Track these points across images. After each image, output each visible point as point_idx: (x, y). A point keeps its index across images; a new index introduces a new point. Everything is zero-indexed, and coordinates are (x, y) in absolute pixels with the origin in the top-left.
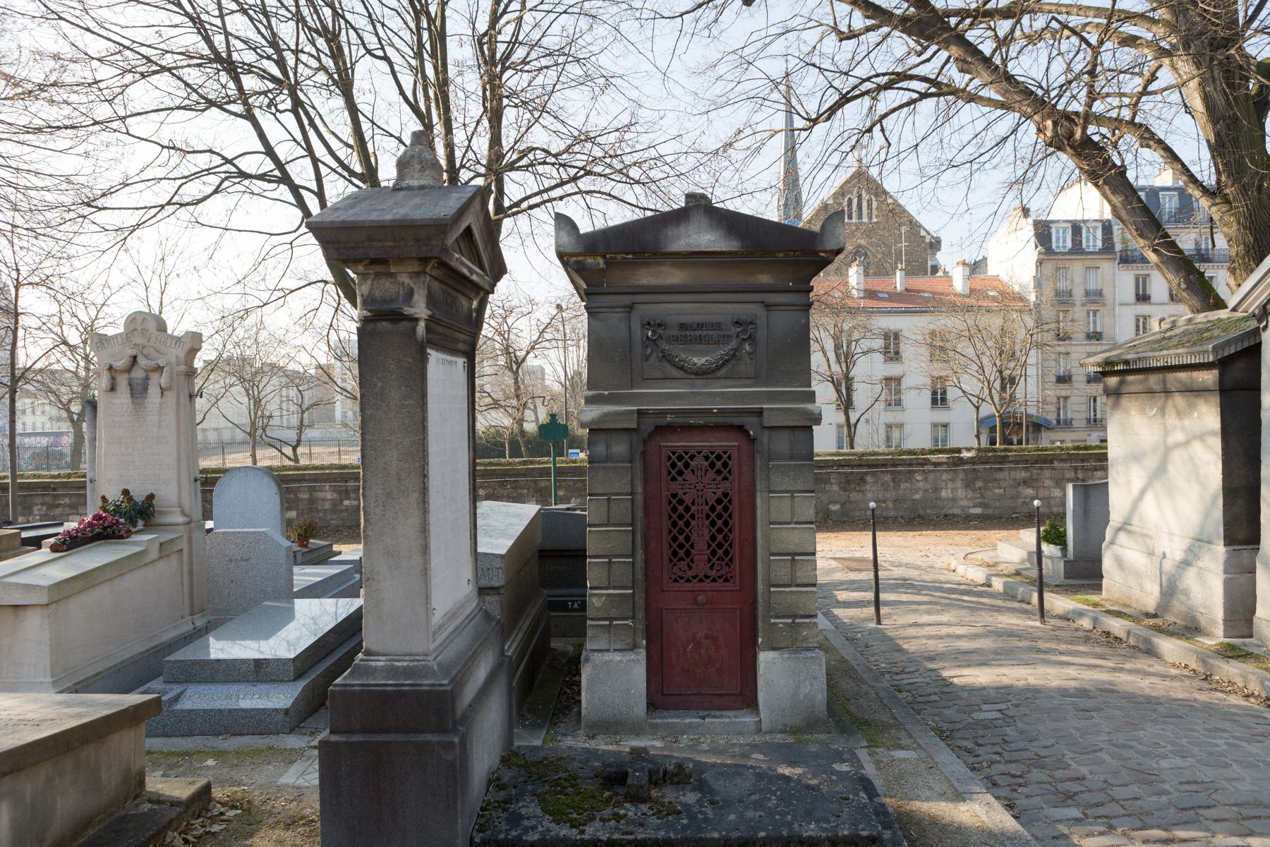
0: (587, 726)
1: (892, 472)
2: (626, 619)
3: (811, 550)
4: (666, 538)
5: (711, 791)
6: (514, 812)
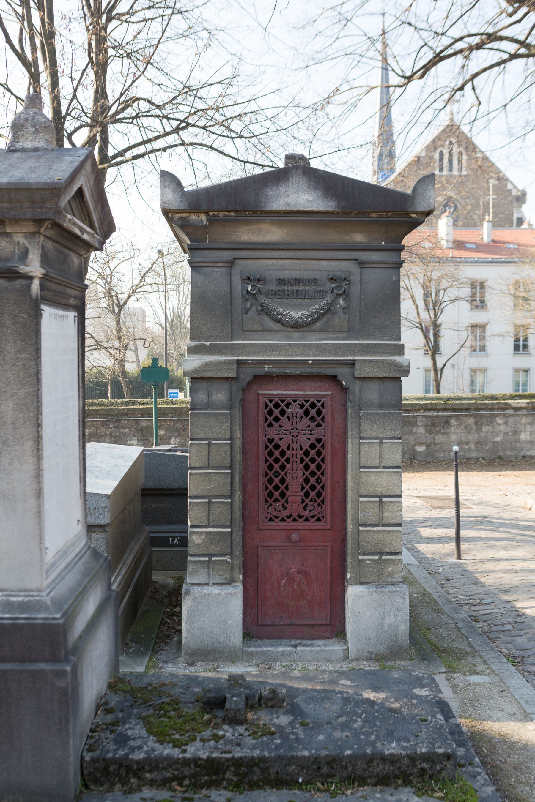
0: (187, 654)
1: (475, 416)
2: (225, 555)
3: (397, 492)
4: (263, 480)
5: (302, 714)
6: (121, 734)
